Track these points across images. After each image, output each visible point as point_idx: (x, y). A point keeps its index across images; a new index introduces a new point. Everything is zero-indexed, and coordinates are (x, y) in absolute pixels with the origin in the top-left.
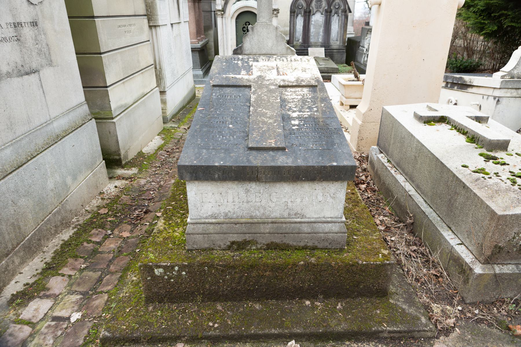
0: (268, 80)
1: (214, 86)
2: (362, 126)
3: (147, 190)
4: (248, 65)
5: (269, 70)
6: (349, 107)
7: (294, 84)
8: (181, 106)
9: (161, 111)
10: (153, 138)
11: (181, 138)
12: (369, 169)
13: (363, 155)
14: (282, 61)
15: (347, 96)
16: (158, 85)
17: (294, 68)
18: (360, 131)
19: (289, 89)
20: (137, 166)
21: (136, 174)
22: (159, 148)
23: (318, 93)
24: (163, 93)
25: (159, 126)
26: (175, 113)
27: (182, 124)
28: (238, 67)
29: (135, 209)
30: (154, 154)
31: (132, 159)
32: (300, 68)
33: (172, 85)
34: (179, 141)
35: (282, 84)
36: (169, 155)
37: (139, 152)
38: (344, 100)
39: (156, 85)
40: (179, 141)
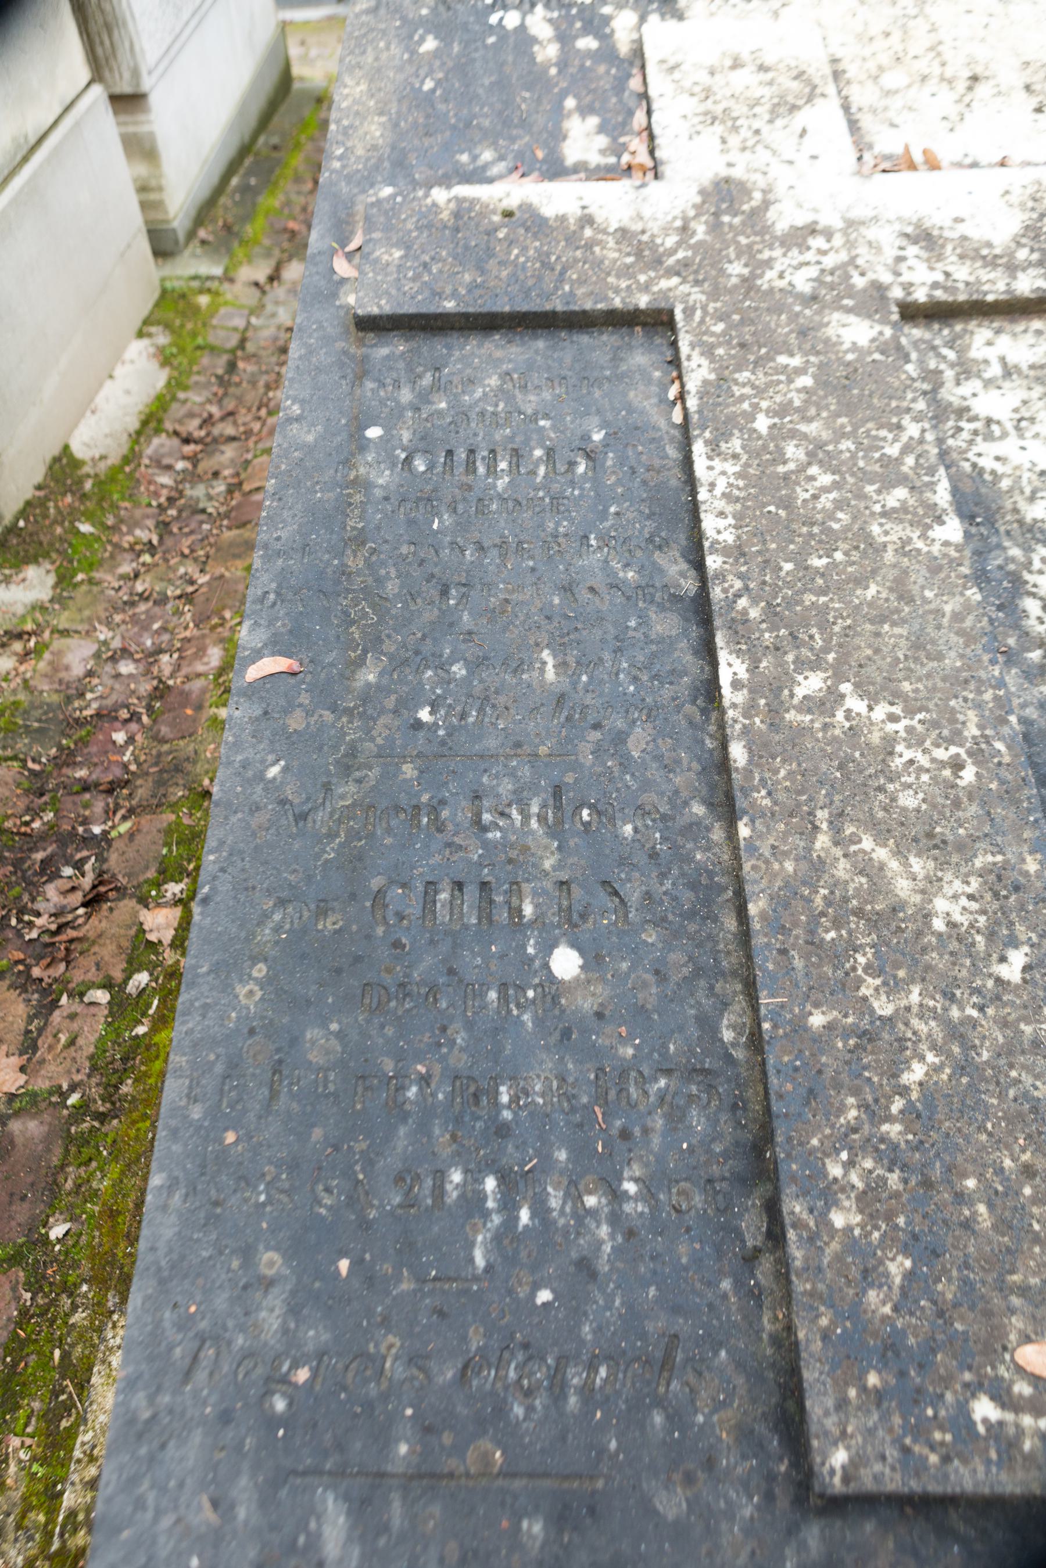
0: (799, 237)
1: (370, 325)
3: (98, 715)
4: (608, 53)
5: (784, 107)
8: (231, 151)
9: (132, 201)
10: (117, 357)
11: (243, 341)
16: (99, 65)
19: (984, 342)
20: (47, 555)
21: (43, 608)
22: (145, 423)
24: (128, 102)
25: (139, 279)
26: (205, 193)
27: (240, 252)
28: (535, 78)
29: (49, 870)
30: (126, 460)
31: (23, 513)
33: (171, 53)
34: (232, 367)
35: (922, 280)
36: (194, 460)
37: (56, 460)
39: (84, 74)
40: (232, 367)
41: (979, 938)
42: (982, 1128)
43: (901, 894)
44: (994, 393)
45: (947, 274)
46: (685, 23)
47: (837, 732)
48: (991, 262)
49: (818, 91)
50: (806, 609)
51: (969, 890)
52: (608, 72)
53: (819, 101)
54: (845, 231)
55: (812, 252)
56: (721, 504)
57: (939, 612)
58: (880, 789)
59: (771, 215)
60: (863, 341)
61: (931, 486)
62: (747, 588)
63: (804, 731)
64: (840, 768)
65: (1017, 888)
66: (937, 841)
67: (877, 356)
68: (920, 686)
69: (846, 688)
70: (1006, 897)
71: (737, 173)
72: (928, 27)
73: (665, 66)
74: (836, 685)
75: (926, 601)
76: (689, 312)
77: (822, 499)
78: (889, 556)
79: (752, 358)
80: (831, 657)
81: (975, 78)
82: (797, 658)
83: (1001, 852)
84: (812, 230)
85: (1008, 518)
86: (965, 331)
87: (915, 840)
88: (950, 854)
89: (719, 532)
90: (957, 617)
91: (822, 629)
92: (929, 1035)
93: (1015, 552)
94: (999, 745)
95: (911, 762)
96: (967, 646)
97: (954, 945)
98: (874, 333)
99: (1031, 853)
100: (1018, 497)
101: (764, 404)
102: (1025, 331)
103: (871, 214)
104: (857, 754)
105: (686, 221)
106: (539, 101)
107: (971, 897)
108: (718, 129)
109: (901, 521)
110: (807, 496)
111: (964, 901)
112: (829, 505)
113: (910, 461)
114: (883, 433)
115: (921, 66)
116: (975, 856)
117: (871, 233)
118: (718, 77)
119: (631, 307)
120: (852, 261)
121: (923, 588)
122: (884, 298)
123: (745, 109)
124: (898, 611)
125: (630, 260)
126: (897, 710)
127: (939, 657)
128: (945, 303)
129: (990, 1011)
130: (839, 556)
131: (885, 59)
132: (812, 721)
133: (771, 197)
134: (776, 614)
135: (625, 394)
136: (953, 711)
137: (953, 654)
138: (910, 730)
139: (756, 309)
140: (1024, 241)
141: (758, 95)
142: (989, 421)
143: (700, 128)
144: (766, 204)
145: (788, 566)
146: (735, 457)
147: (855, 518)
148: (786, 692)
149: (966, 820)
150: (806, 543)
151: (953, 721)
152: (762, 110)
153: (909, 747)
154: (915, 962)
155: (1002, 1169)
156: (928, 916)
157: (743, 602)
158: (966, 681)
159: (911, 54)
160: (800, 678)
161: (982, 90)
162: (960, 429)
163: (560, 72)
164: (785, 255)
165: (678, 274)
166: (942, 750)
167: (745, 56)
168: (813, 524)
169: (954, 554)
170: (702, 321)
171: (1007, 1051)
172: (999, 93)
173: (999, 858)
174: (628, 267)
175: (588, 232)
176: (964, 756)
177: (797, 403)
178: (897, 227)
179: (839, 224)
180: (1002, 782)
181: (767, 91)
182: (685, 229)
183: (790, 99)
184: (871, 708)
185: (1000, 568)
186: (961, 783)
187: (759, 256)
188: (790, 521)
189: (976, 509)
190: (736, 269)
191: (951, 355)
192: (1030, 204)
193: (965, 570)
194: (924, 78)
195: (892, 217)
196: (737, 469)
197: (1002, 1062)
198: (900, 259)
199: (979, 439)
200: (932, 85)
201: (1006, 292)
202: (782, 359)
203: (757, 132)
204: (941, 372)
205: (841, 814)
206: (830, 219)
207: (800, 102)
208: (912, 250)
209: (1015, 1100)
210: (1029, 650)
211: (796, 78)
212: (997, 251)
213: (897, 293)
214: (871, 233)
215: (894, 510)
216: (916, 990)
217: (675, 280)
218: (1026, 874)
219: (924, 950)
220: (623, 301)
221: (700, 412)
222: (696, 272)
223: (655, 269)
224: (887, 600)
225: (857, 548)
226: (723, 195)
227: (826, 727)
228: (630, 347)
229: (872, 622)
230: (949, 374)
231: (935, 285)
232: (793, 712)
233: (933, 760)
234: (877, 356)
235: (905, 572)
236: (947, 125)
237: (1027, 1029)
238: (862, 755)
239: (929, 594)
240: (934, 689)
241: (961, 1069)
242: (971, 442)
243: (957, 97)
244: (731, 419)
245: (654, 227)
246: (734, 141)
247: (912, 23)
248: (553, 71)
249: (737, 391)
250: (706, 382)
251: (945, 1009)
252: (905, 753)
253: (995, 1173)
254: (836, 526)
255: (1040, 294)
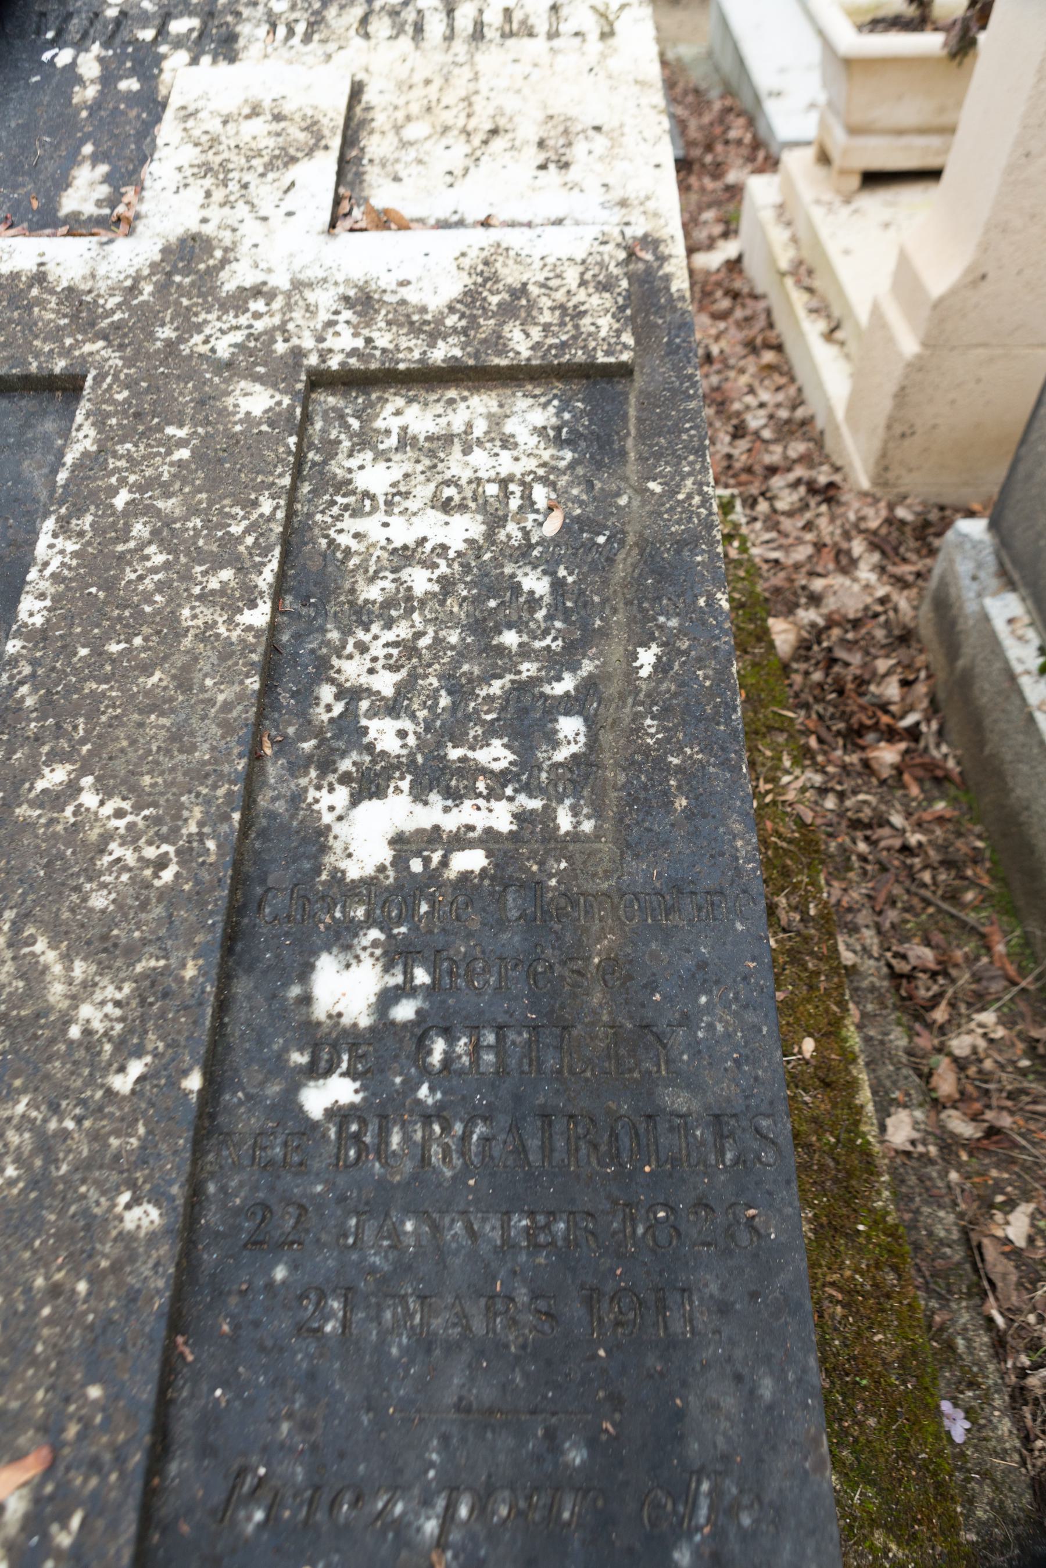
2: (917, 366)
6: (855, 181)
7: (440, 354)
12: (927, 631)
13: (901, 513)
14: (405, 42)
15: (858, 118)
17: (482, 123)
18: (901, 395)
23: (632, 469)
32: (529, 131)
38: (838, 139)
41: (108, 1047)
42: (29, 1246)
43: (52, 999)
44: (382, 465)
45: (369, 341)
46: (237, 64)
47: (59, 828)
48: (415, 329)
49: (323, 143)
50: (83, 697)
51: (119, 996)
52: (138, 116)
53: (319, 154)
54: (288, 295)
55: (248, 315)
56: (45, 585)
57: (212, 702)
58: (77, 889)
59: (223, 275)
60: (257, 411)
61: (258, 569)
62: (34, 675)
63: (29, 825)
64: (46, 866)
65: (166, 995)
66: (108, 944)
67: (264, 428)
68: (160, 780)
69: (87, 781)
70: (151, 1004)
71: (208, 230)
72: (471, 75)
73: (183, 113)
74: (78, 778)
75: (203, 689)
76: (98, 380)
77: (147, 581)
78: (187, 642)
79: (141, 428)
80: (85, 749)
81: (494, 132)
82: (52, 749)
83: (166, 957)
84: (257, 291)
85: (342, 598)
86: (380, 398)
87: (88, 943)
88: (116, 958)
89: (31, 615)
90: (227, 707)
91: (89, 718)
92: (19, 1147)
93: (334, 635)
94: (211, 845)
95: (119, 860)
96: (223, 737)
97: (80, 1054)
98: (272, 403)
99: (194, 958)
100: (360, 578)
101: (132, 478)
102: (438, 401)
103: (321, 274)
104: (69, 852)
105: (137, 279)
106: (56, 147)
107: (118, 1004)
108: (208, 182)
109: (214, 604)
110: (133, 576)
111: (109, 1008)
112: (151, 587)
113: (250, 540)
114: (237, 510)
115: (447, 117)
116: (139, 960)
117: (311, 296)
118: (229, 126)
119: (45, 373)
120: (282, 328)
121: (206, 675)
122: (298, 365)
123: (243, 160)
124: (172, 699)
125: (64, 322)
126: (126, 805)
127: (193, 748)
128: (358, 370)
129: (87, 1124)
130: (138, 641)
131: (415, 109)
132: (39, 816)
133: (231, 255)
134: (51, 702)
135: (19, 463)
136: (182, 807)
137: (206, 746)
138: (131, 827)
139: (167, 376)
140: (459, 306)
141: (261, 146)
142: (366, 494)
143: (190, 180)
144: (224, 262)
145: (83, 652)
146: (81, 534)
147: (170, 601)
148: (27, 785)
149: (146, 924)
150: (112, 627)
151: (177, 817)
152: (258, 163)
153: (121, 845)
154: (37, 1069)
155: (31, 1289)
156: (66, 1021)
157: (24, 689)
158: (207, 776)
159: (443, 104)
160: (46, 771)
161: (498, 144)
162: (333, 503)
163: (90, 115)
164: (219, 319)
165: (105, 338)
166: (153, 848)
167: (267, 104)
168: (126, 607)
169: (251, 640)
170: (110, 387)
171: (84, 1167)
172: (512, 147)
173: (162, 963)
174: (59, 328)
175: (35, 292)
176: (172, 855)
177: (166, 477)
178: (341, 290)
179: (286, 286)
180: (198, 882)
181: (271, 142)
182: (133, 290)
183: (292, 151)
184: (102, 803)
185: (313, 651)
186: (157, 883)
187: (194, 319)
188: (105, 603)
189: (313, 589)
190: (166, 333)
191: (355, 424)
192: (480, 267)
193: (255, 657)
194: (446, 129)
195: (341, 278)
196: (77, 547)
197: (78, 1176)
198: (331, 324)
199: (347, 514)
200: (449, 139)
201: (420, 361)
202: (170, 430)
203: (245, 186)
204: (340, 442)
205: (27, 915)
206: (281, 281)
207: (300, 155)
208: (347, 314)
209: (73, 1216)
210: (305, 740)
211: (307, 129)
212: (428, 317)
213: (313, 360)
214: (311, 296)
215: (213, 592)
216: (25, 1100)
217: (101, 343)
218: (180, 980)
219: (49, 1059)
220: (39, 367)
221: (65, 486)
222: (125, 335)
223: (85, 332)
224: (166, 688)
225: (158, 633)
226: (189, 253)
227: (52, 821)
228: (45, 413)
229: (141, 712)
230: (346, 444)
231: (354, 352)
232: (25, 806)
233: (141, 859)
234: (264, 428)
235: (196, 659)
236: (449, 179)
237: (114, 1142)
238: (74, 853)
239: (209, 682)
240: (173, 783)
241: (34, 1183)
242: (338, 518)
243: (469, 151)
244: (93, 494)
245: (102, 286)
246: (218, 195)
247: (456, 71)
248: (84, 114)
249: (112, 463)
250: (85, 454)
251: (45, 1121)
252: (116, 850)
253: (23, 1293)
254: (148, 609)
255: (452, 363)
